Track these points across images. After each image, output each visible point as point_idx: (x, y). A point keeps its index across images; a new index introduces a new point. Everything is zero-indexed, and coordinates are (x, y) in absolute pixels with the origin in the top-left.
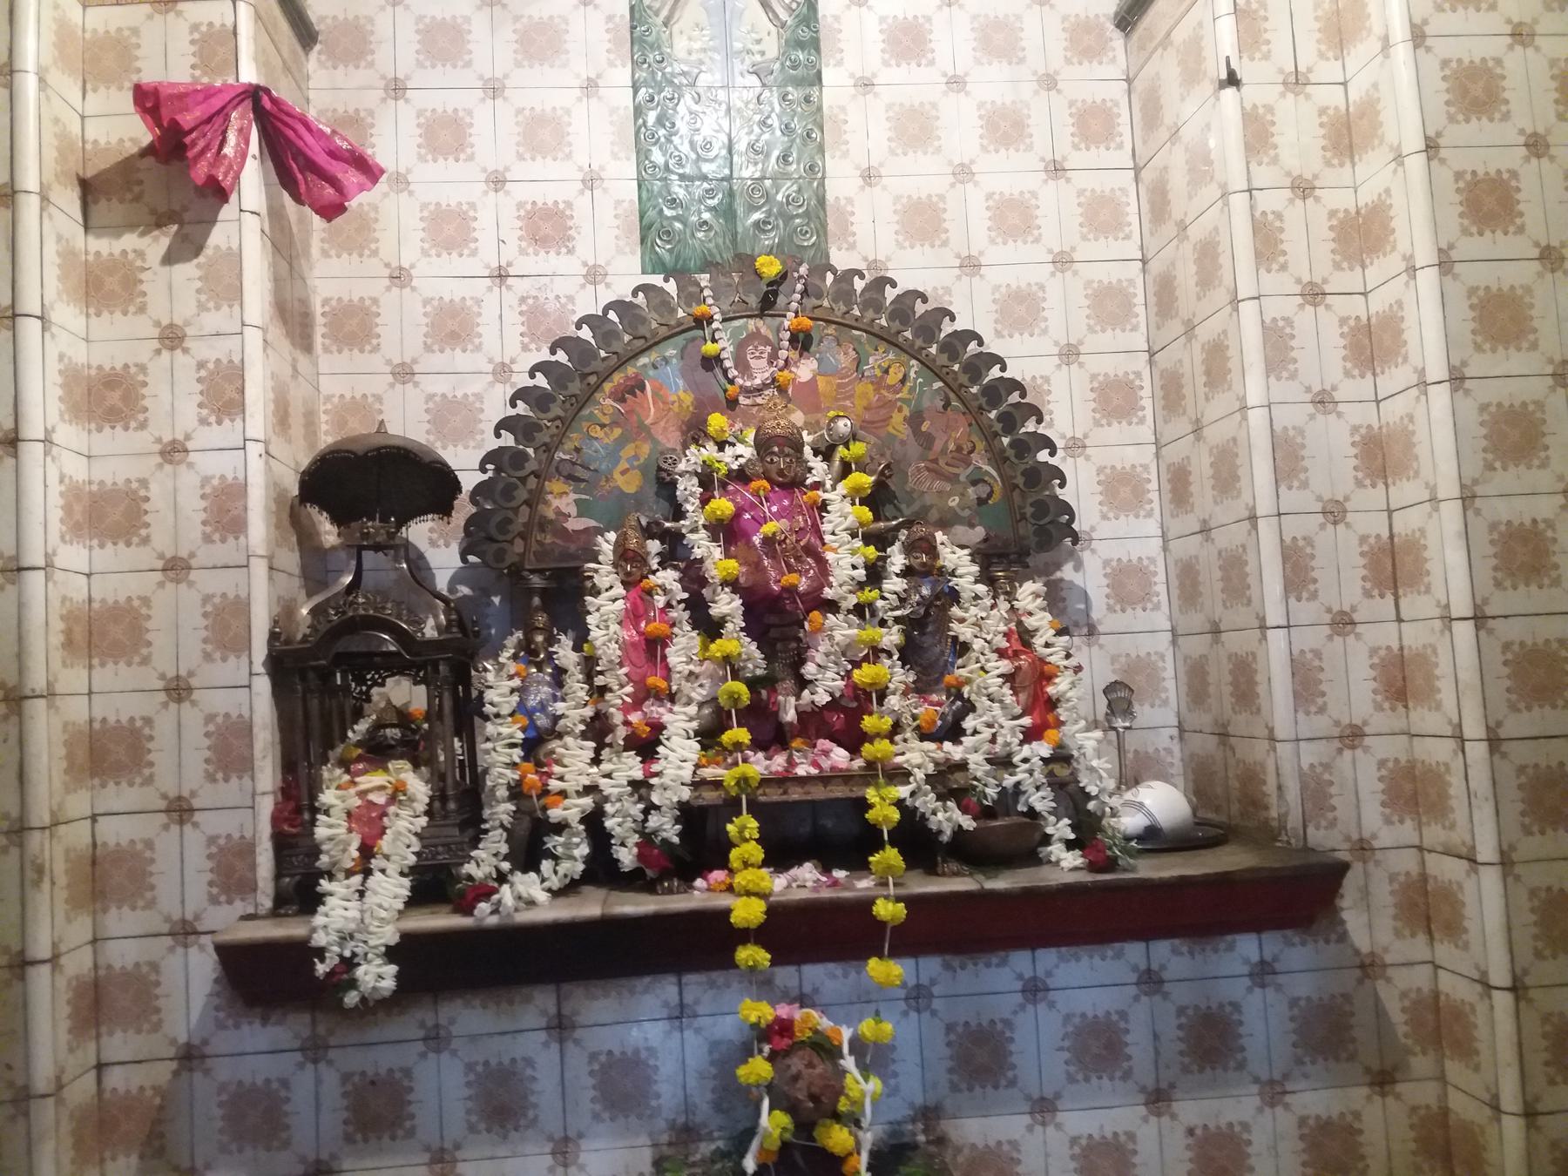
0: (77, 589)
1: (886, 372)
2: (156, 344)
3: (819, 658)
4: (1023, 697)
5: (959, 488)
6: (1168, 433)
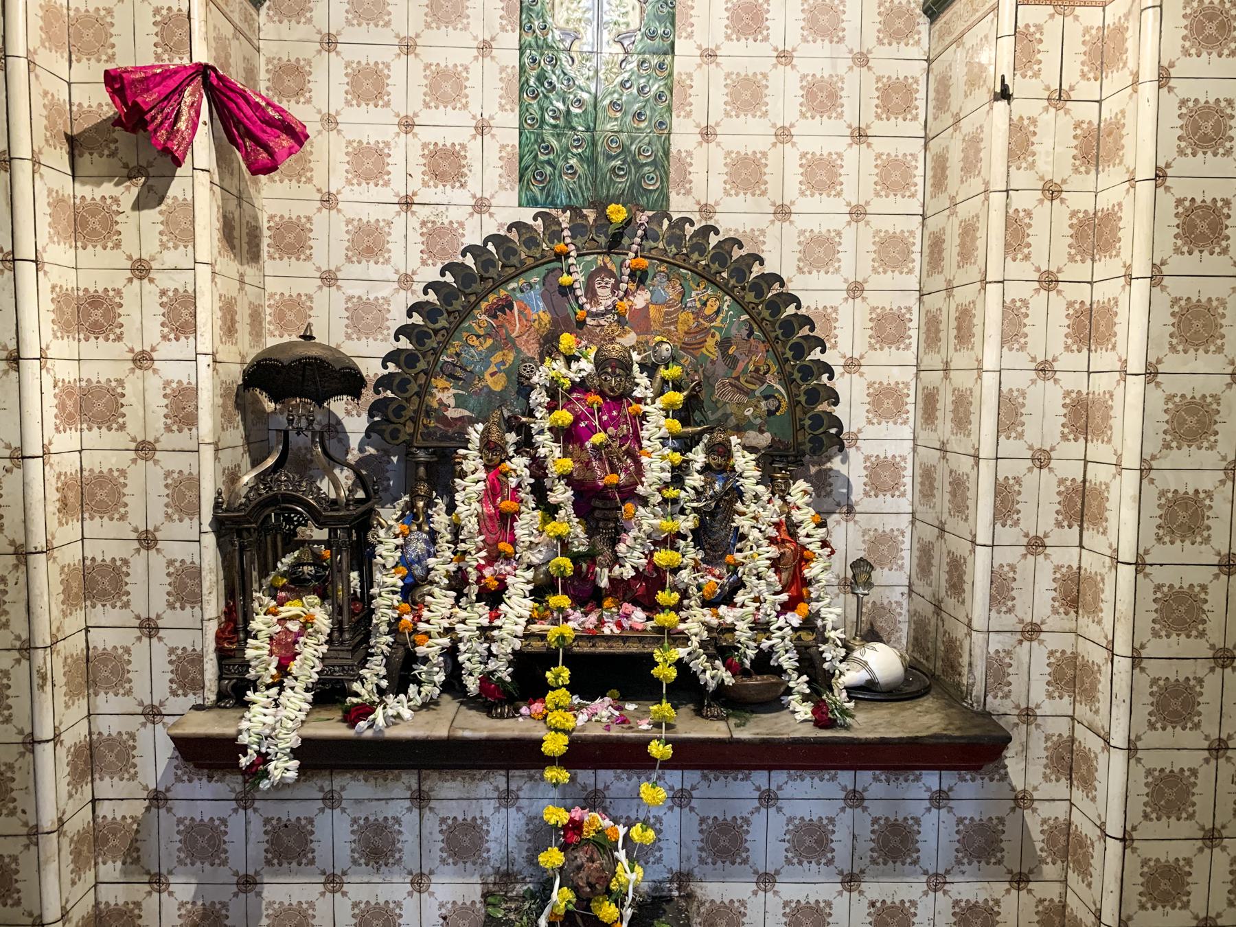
0: (70, 464)
1: (705, 304)
2: (129, 274)
3: (629, 541)
4: (784, 575)
5: (754, 401)
6: (927, 361)
